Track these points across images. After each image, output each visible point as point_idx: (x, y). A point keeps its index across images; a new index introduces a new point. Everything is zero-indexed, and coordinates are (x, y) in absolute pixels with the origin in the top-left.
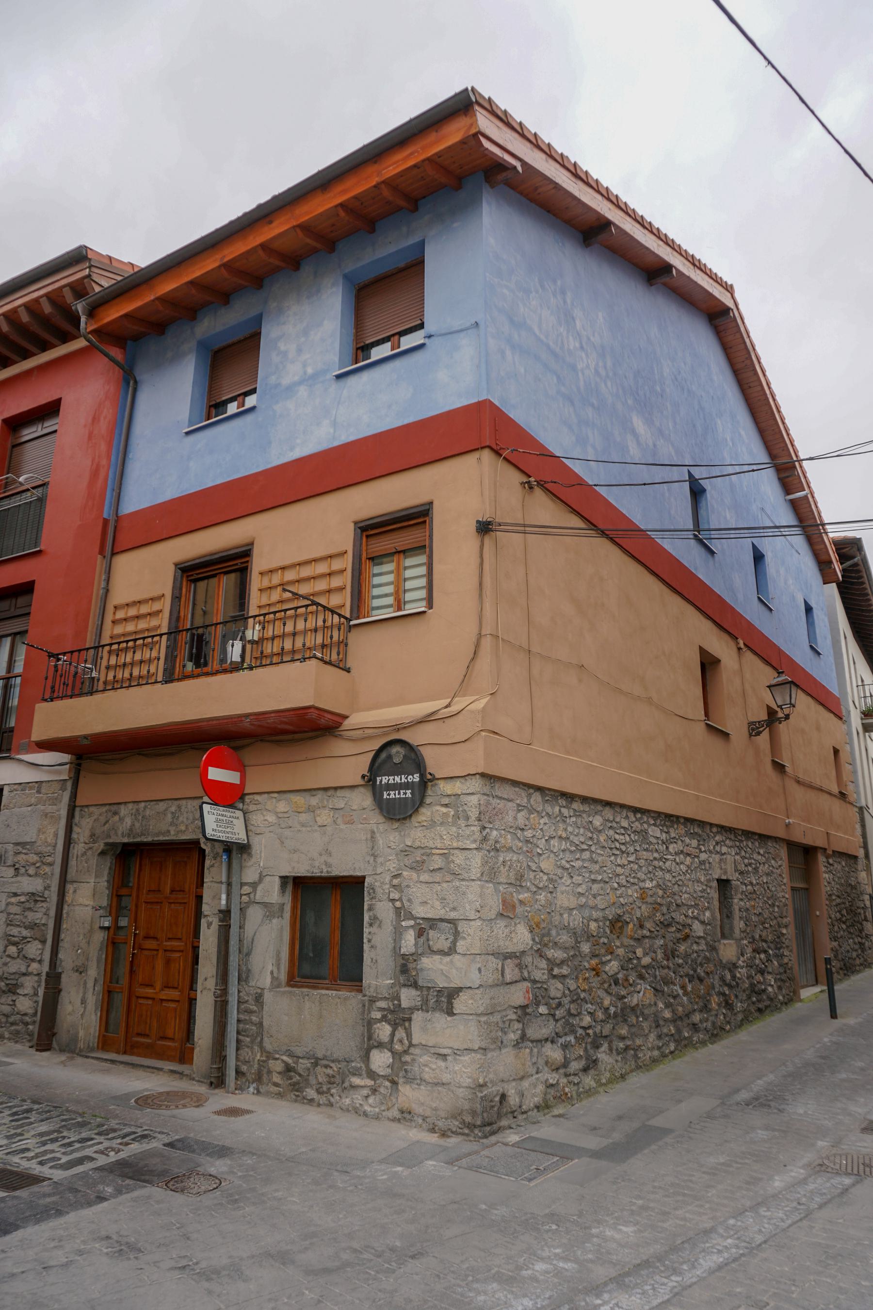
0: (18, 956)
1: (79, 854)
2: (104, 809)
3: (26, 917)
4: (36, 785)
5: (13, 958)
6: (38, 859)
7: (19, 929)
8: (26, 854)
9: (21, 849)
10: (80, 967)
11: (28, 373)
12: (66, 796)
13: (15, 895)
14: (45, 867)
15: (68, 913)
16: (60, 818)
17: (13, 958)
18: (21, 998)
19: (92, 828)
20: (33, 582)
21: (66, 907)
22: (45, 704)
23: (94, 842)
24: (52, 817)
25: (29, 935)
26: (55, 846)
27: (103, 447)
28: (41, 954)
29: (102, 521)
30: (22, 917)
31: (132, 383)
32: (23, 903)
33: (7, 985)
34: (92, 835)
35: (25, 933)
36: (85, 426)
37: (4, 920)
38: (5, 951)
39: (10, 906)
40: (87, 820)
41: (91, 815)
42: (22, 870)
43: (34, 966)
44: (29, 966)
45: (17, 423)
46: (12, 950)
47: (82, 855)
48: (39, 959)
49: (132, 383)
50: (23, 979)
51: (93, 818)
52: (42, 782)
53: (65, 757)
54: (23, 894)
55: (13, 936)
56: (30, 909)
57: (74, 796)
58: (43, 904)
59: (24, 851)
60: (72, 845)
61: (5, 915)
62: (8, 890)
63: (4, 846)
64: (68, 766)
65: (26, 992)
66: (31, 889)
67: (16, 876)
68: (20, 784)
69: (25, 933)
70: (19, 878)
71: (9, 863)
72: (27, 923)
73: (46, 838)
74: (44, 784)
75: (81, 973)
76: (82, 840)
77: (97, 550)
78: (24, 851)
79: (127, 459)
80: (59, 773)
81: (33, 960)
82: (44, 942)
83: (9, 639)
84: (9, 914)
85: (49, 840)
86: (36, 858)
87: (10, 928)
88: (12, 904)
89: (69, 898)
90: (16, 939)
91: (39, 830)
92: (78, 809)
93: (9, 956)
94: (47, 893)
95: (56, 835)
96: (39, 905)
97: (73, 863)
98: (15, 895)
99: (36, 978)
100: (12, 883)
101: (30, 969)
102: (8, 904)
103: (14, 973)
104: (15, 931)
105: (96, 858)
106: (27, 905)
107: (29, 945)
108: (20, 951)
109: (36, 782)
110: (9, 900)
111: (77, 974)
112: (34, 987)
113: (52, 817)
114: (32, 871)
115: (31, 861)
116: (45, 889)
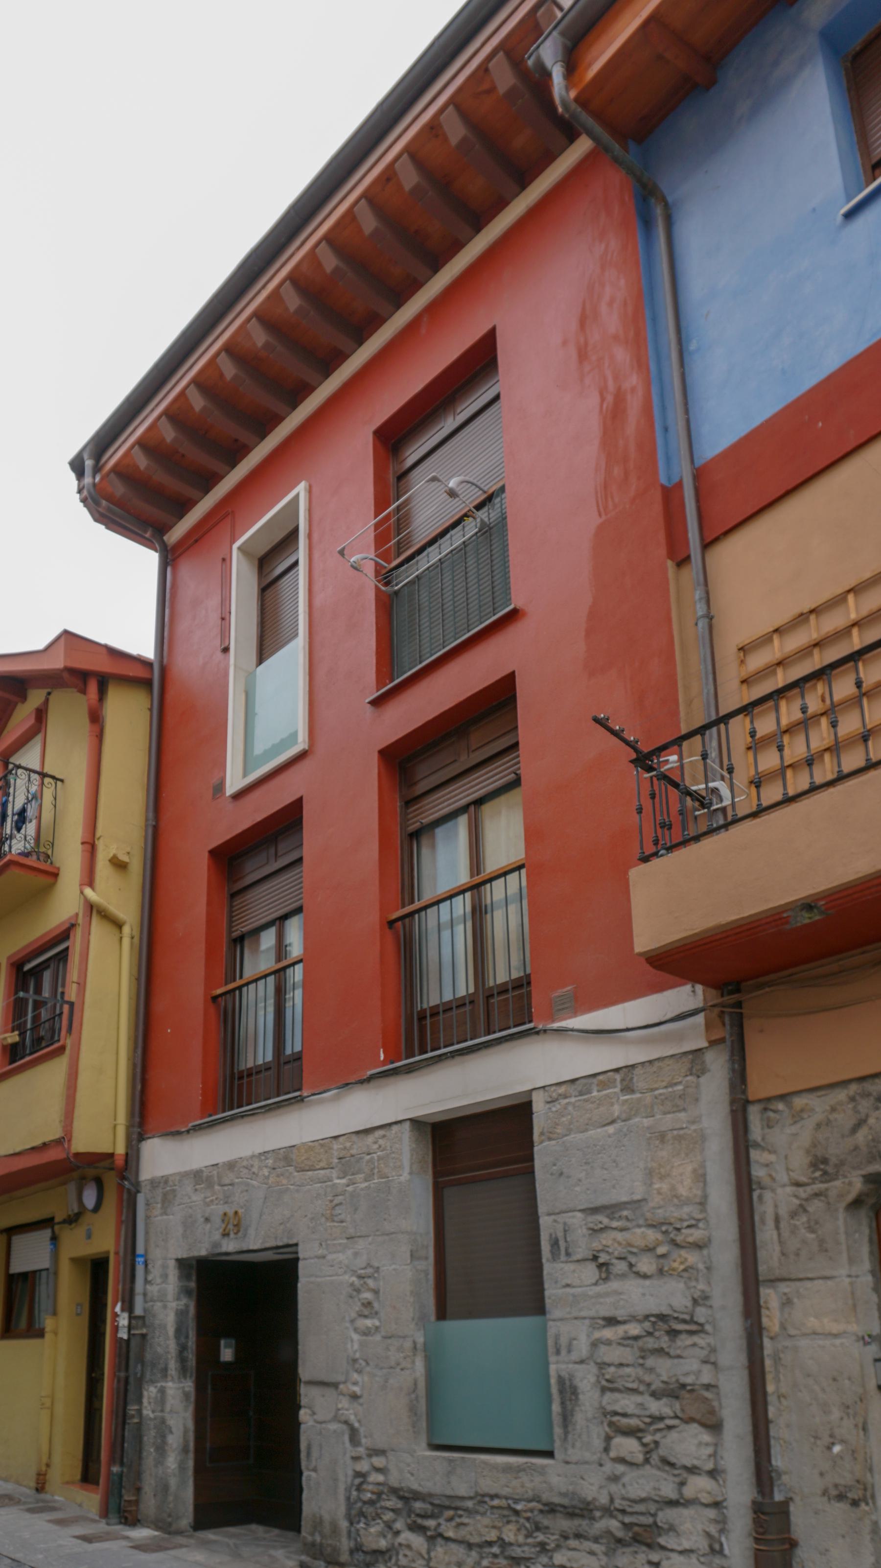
0: (647, 1461)
1: (783, 1212)
2: (841, 1095)
3: (651, 1370)
4: (618, 1077)
5: (632, 1464)
6: (660, 1236)
7: (639, 1399)
8: (622, 1230)
9: (606, 1221)
10: (850, 1488)
11: (413, 326)
12: (714, 1085)
13: (611, 1321)
14: (683, 1253)
15: (777, 1360)
16: (702, 1137)
17: (632, 1464)
18: (676, 1558)
19: (814, 1145)
20: (511, 676)
21: (768, 1346)
22: (643, 867)
23: (827, 1177)
24: (679, 1138)
25: (667, 1411)
26: (703, 1204)
27: (622, 355)
28: (714, 1455)
29: (658, 496)
30: (640, 1371)
31: (659, 211)
32: (636, 1338)
33: (626, 1526)
34: (819, 1162)
35: (656, 1407)
36: (565, 343)
37: (593, 1379)
38: (606, 1450)
39: (603, 1349)
40: (790, 1130)
41: (798, 1116)
42: (620, 1267)
43: (698, 1486)
44: (682, 1484)
45: (12, 1231)
46: (628, 1446)
47: (793, 1215)
48: (710, 1466)
49: (659, 211)
50: (666, 1516)
51: (809, 1123)
52: (633, 1066)
53: (685, 996)
54: (633, 1318)
55: (625, 1415)
56: (660, 1352)
57: (739, 1078)
58: (695, 1339)
59: (615, 1224)
60: (755, 1195)
61: (594, 1369)
62: (592, 1313)
63: (561, 1218)
64: (700, 1019)
65: (686, 1545)
66: (654, 1305)
67: (606, 1279)
68: (573, 1081)
69: (656, 1407)
70: (614, 1285)
71: (581, 1252)
72: (657, 1385)
73: (673, 1188)
74: (638, 1071)
75: (855, 1503)
76: (782, 1177)
77: (662, 551)
78: (615, 1224)
79: (685, 354)
80: (679, 1037)
81: (693, 1470)
82: (715, 1427)
83: (463, 822)
84: (602, 1366)
85: (683, 1191)
86: (652, 1235)
87: (608, 1396)
88: (608, 1343)
89: (772, 1320)
90: (634, 1422)
91: (650, 1173)
92: (754, 1112)
93: (622, 1460)
94: (701, 1314)
95: (701, 1177)
96: (685, 1341)
97: (766, 1235)
98: (611, 1321)
99: (712, 1513)
100: (599, 1295)
101: (689, 1492)
102: (595, 1344)
103: (642, 1500)
104: (626, 1403)
105: (841, 1215)
106: (651, 1343)
107: (674, 1435)
108: (649, 1450)
109: (617, 1070)
110: (597, 1335)
111: (843, 1506)
112: (708, 1534)
113: (679, 1138)
114: (646, 1265)
115: (641, 1243)
116: (695, 1302)
